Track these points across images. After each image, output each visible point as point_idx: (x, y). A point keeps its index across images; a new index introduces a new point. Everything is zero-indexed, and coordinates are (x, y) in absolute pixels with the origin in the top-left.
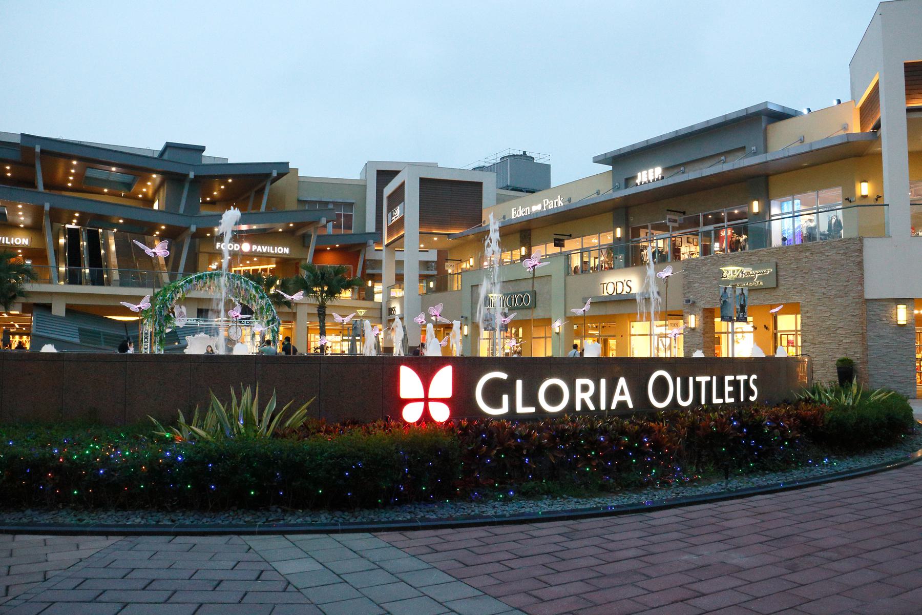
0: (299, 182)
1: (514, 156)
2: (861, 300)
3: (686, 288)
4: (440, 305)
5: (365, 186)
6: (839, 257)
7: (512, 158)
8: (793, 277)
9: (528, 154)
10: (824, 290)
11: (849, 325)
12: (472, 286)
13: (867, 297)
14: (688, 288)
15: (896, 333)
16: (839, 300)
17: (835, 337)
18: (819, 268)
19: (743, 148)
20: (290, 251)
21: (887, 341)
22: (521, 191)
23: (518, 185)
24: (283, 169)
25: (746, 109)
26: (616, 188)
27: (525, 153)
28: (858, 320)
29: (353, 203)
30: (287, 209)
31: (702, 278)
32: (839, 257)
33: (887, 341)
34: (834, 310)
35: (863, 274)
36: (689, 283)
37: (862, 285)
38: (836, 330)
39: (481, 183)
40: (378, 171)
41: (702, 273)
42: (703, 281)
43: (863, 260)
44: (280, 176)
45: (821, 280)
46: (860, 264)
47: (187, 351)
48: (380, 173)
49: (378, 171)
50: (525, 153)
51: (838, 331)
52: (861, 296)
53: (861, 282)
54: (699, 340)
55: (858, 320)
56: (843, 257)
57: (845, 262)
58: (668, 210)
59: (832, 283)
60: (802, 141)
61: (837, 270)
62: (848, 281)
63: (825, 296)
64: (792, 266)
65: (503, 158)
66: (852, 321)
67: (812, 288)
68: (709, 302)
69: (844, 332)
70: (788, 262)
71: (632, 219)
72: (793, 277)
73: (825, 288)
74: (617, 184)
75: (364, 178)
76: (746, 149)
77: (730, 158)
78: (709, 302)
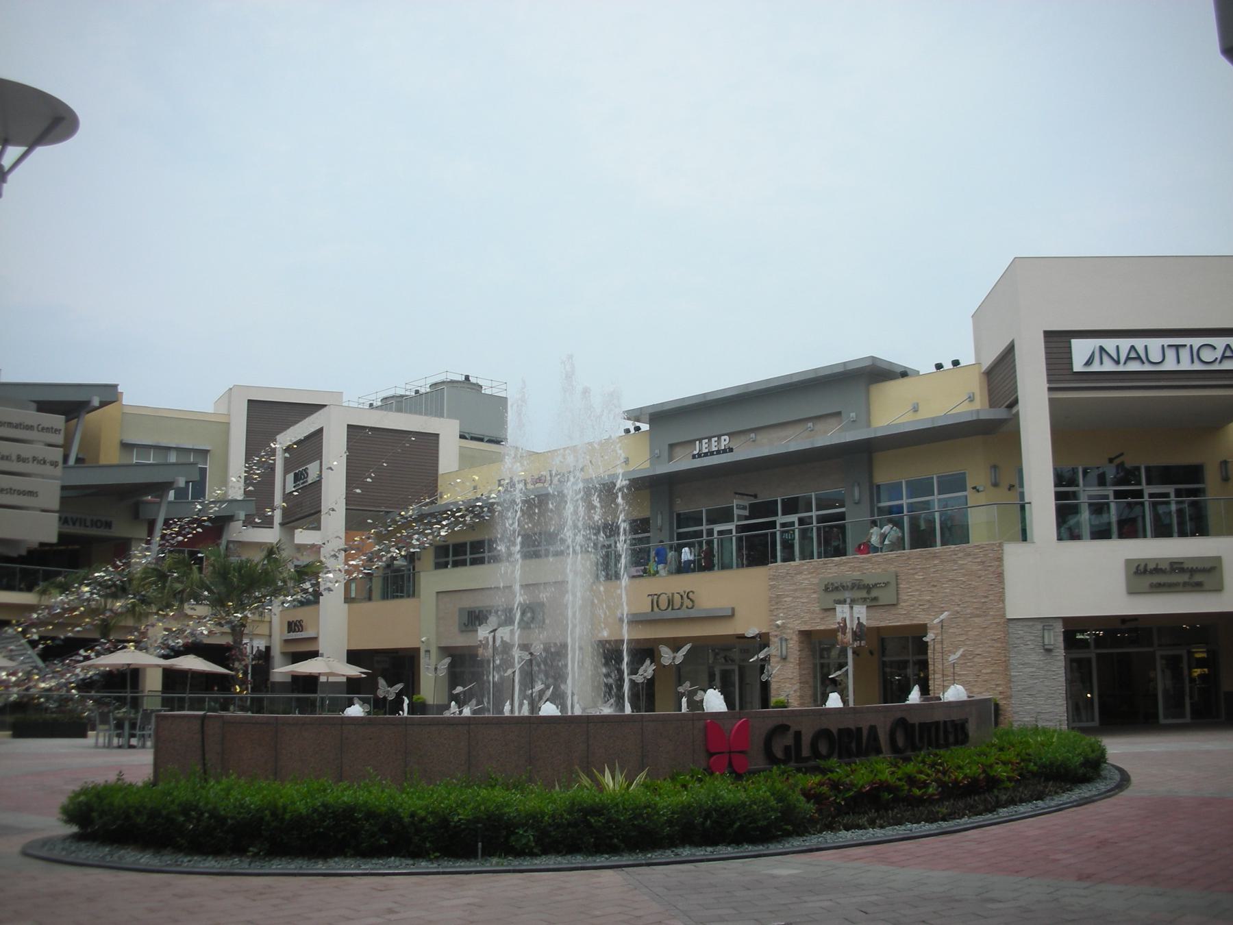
0: (123, 413)
1: (452, 382)
2: (1003, 620)
3: (773, 603)
4: (661, 649)
5: (228, 424)
6: (975, 568)
7: (450, 385)
8: (917, 590)
9: (472, 380)
10: (958, 609)
11: (989, 652)
12: (438, 593)
13: (1009, 616)
14: (777, 603)
15: (1042, 661)
16: (977, 620)
17: (971, 667)
18: (951, 580)
19: (839, 414)
20: (1209, 671)
21: (1034, 670)
22: (481, 440)
23: (477, 432)
24: (109, 394)
25: (845, 364)
26: (655, 458)
27: (467, 378)
28: (999, 645)
29: (207, 451)
30: (103, 461)
31: (796, 590)
32: (975, 568)
33: (1034, 670)
34: (970, 633)
35: (1003, 588)
36: (778, 596)
37: (1003, 601)
38: (974, 657)
39: (438, 434)
40: (249, 401)
41: (795, 584)
42: (797, 594)
43: (1003, 570)
44: (103, 404)
45: (953, 595)
46: (1000, 576)
47: (541, 714)
48: (256, 407)
49: (249, 401)
50: (467, 378)
51: (976, 660)
52: (1004, 615)
53: (1001, 599)
54: (793, 673)
55: (999, 645)
56: (980, 567)
57: (983, 573)
58: (736, 493)
59: (967, 599)
60: (915, 410)
61: (973, 583)
62: (986, 597)
63: (959, 615)
64: (917, 577)
65: (436, 384)
66: (993, 647)
67: (943, 605)
68: (805, 623)
69: (983, 660)
70: (911, 571)
71: (679, 501)
72: (917, 590)
73: (959, 605)
74: (657, 451)
75: (223, 410)
76: (843, 415)
77: (820, 426)
78: (805, 623)
